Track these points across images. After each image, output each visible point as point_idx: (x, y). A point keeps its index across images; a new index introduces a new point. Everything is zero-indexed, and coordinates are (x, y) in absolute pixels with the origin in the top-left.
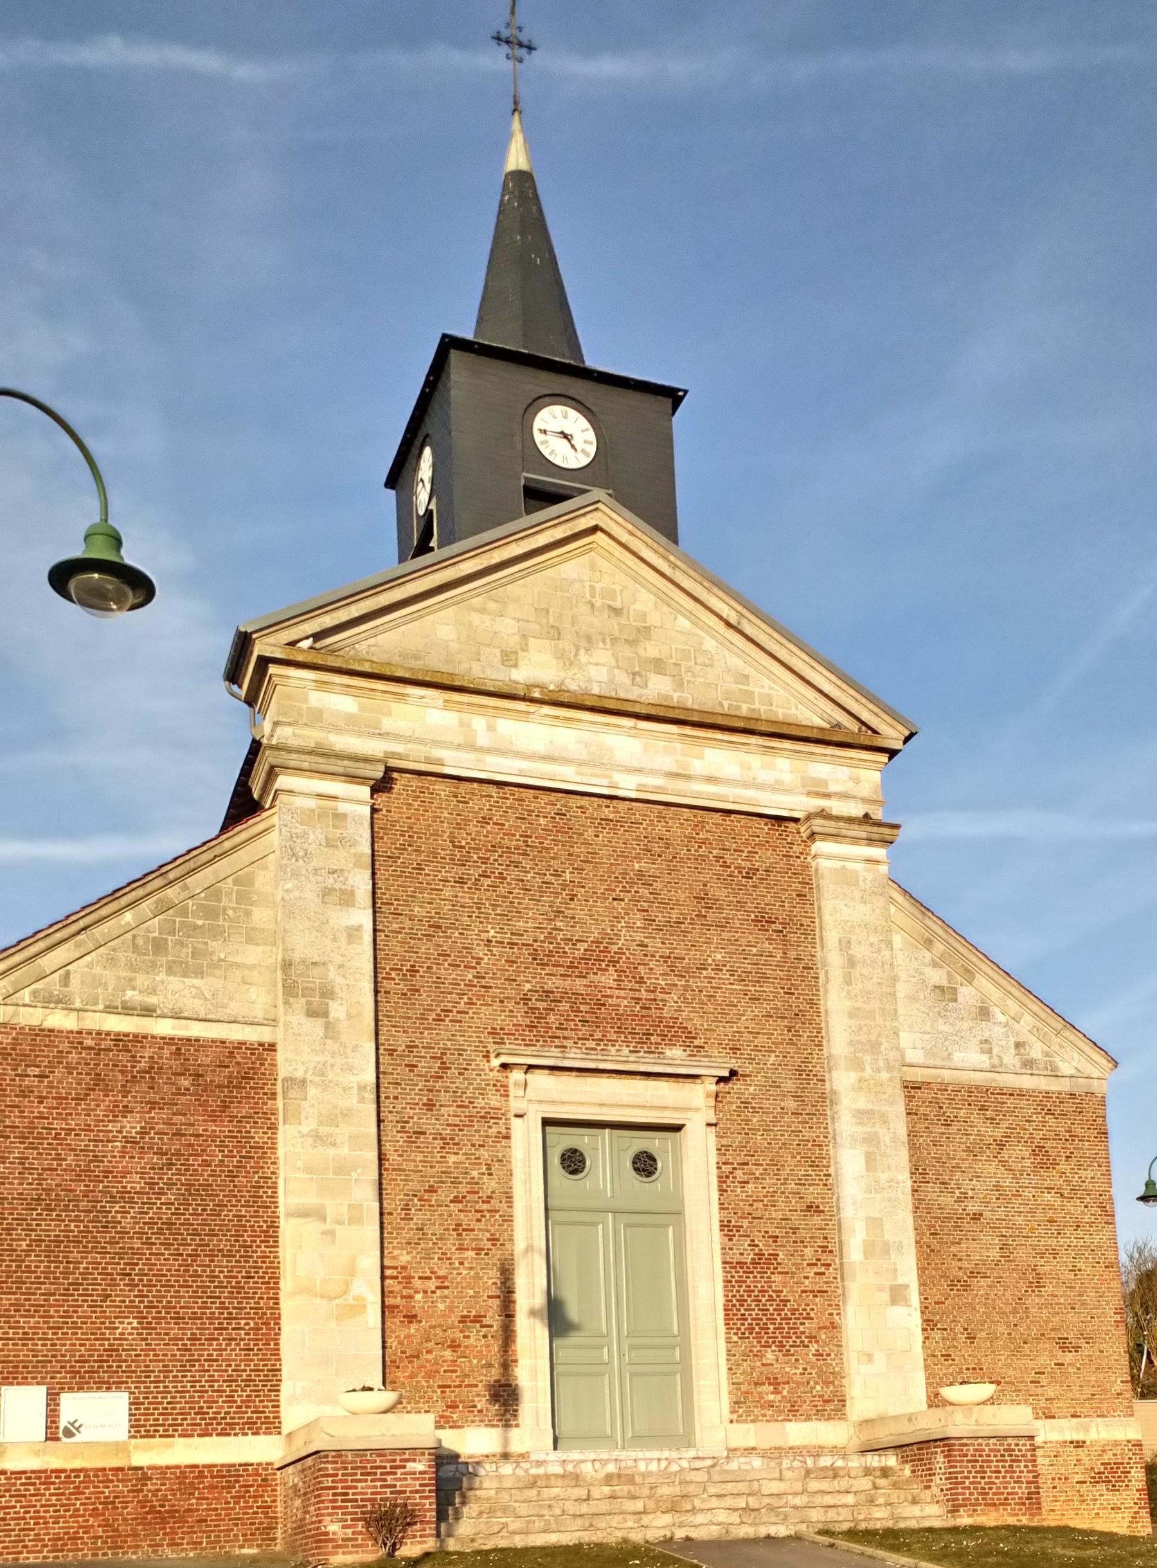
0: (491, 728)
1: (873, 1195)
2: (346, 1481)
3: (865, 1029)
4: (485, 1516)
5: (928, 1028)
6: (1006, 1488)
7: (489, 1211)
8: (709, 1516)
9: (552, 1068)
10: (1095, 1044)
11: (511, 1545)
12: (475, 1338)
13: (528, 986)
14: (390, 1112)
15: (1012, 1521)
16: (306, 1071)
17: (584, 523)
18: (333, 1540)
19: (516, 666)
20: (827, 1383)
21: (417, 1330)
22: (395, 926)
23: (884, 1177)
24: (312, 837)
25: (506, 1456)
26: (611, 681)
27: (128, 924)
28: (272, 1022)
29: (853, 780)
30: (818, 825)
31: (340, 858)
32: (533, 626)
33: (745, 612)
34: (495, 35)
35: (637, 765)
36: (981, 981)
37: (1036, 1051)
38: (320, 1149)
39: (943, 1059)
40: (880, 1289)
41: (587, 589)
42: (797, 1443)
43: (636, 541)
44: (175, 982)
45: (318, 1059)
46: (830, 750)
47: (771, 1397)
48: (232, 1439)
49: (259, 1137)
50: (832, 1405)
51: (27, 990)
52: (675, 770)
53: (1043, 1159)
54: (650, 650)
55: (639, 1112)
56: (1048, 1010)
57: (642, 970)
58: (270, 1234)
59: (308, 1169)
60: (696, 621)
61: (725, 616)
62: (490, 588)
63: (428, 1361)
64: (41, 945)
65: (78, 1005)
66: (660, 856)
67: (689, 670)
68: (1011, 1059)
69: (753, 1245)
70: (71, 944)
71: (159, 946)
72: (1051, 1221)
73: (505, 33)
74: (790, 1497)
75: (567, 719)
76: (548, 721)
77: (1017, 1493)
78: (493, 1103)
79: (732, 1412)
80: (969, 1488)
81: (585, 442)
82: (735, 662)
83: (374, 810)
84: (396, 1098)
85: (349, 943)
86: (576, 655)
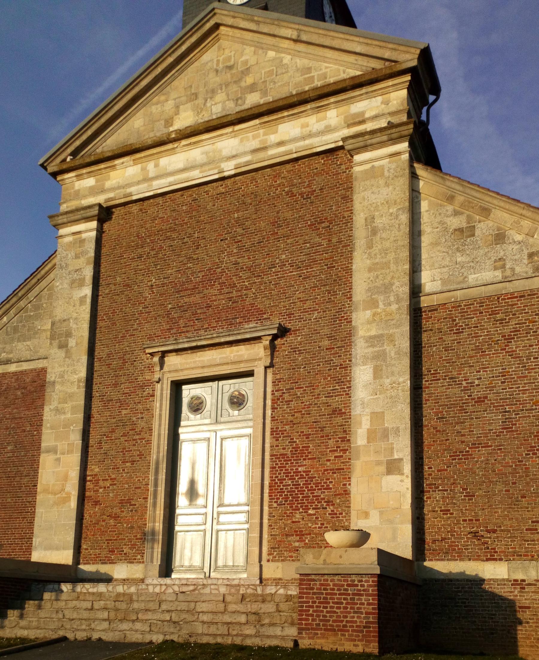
3: (381, 277)
7: (140, 439)
14: (97, 391)
16: (55, 377)
17: (208, 26)
21: (99, 509)
23: (387, 381)
27: (5, 322)
33: (301, 27)
39: (459, 283)
40: (379, 463)
44: (20, 346)
45: (61, 369)
47: (297, 544)
54: (249, 80)
55: (225, 367)
61: (289, 36)
63: (102, 526)
66: (251, 204)
69: (292, 442)
76: (186, 148)
78: (148, 377)
80: (312, 615)
82: (301, 62)
85: (80, 306)
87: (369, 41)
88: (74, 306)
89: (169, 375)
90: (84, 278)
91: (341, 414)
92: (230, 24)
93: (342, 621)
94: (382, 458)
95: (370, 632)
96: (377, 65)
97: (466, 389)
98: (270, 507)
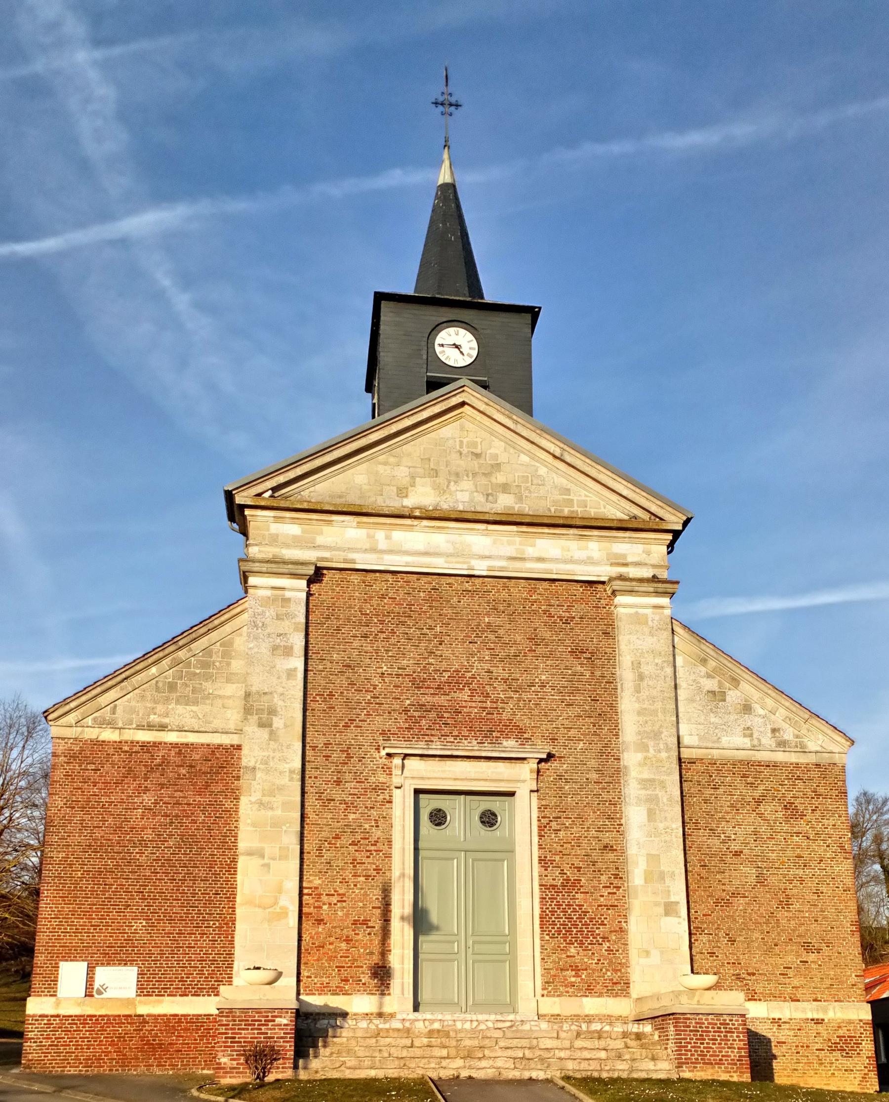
0: (388, 537)
1: (652, 839)
2: (234, 1029)
3: (650, 723)
4: (335, 1055)
5: (702, 720)
6: (720, 1052)
7: (376, 851)
8: (491, 1062)
9: (422, 756)
10: (836, 728)
11: (342, 1077)
12: (362, 935)
13: (408, 702)
15: (724, 1077)
17: (454, 401)
18: (224, 1068)
19: (406, 496)
20: (616, 971)
22: (321, 667)
23: (661, 826)
24: (268, 614)
25: (380, 1015)
26: (472, 500)
28: (239, 732)
29: (645, 554)
30: (617, 585)
31: (285, 626)
32: (419, 470)
33: (565, 447)
34: (434, 101)
35: (487, 553)
36: (744, 686)
37: (788, 734)
38: (263, 811)
39: (714, 742)
40: (656, 904)
41: (458, 443)
42: (591, 1013)
43: (491, 409)
44: (180, 709)
45: (264, 754)
46: (628, 534)
47: (573, 979)
48: (201, 998)
49: (228, 805)
50: (619, 986)
51: (90, 718)
52: (514, 555)
53: (792, 811)
54: (500, 478)
56: (797, 705)
57: (488, 688)
58: (232, 867)
59: (254, 825)
60: (533, 457)
62: (391, 449)
63: (329, 949)
64: (99, 690)
65: (120, 725)
67: (527, 488)
68: (768, 741)
69: (562, 873)
70: (118, 688)
71: (172, 687)
72: (799, 857)
73: (441, 99)
74: (557, 1051)
75: (439, 527)
76: (427, 530)
77: (730, 1056)
78: (381, 780)
79: (543, 989)
80: (691, 1051)
81: (470, 348)
83: (309, 594)
84: (316, 777)
85: (288, 679)
86: (448, 487)
87: (638, 490)
88: (279, 678)
89: (411, 781)
90: (292, 648)
91: (613, 850)
92: (481, 409)
93: (718, 1056)
94: (660, 899)
95: (743, 1064)
96: (645, 516)
97: (724, 842)
98: (542, 939)
